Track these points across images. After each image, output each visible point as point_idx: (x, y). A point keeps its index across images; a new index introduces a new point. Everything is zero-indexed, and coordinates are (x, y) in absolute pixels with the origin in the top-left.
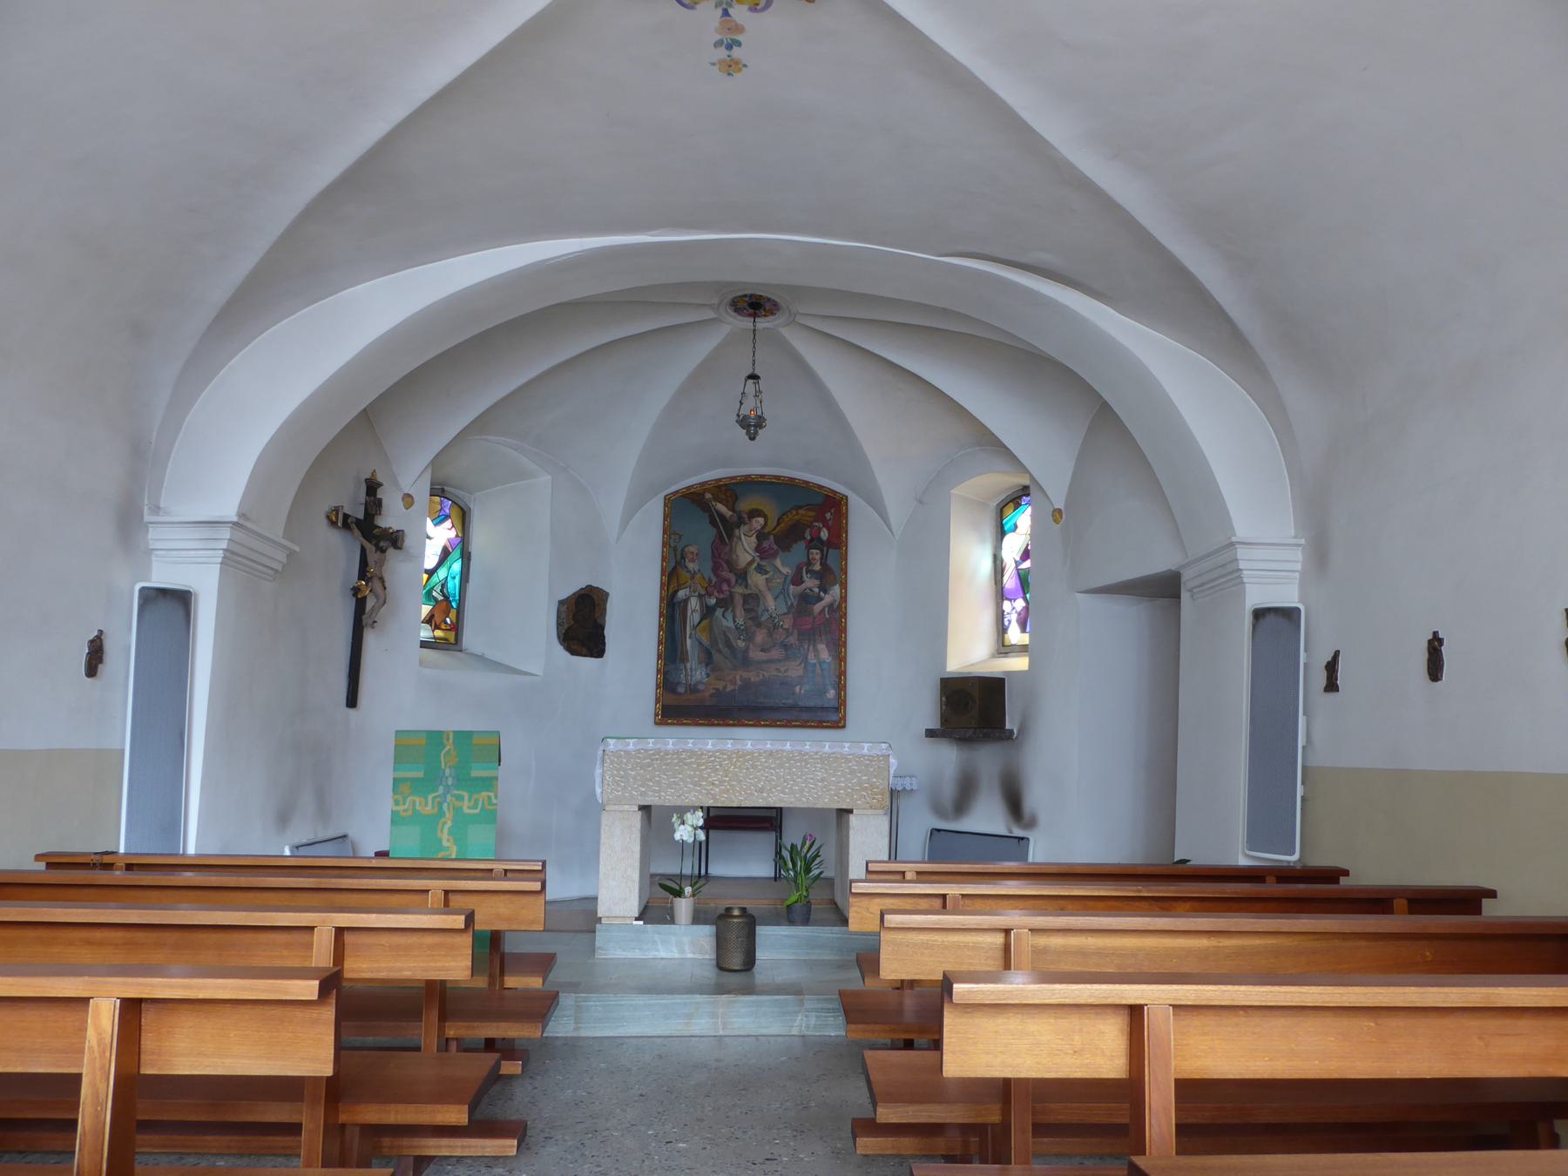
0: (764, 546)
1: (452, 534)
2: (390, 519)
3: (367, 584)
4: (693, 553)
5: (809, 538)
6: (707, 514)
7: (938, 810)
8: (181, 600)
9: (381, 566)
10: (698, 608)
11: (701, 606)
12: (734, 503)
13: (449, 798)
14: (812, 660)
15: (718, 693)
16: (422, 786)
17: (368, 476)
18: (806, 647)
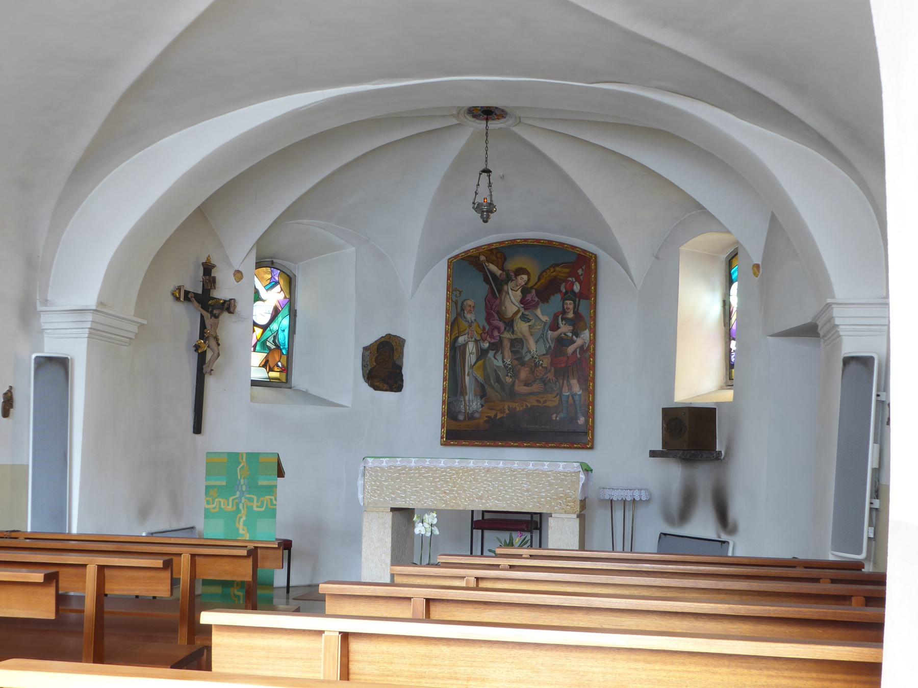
0: (527, 298)
1: (281, 296)
2: (222, 293)
3: (205, 342)
4: (470, 306)
5: (564, 291)
6: (481, 274)
7: (668, 519)
8: (62, 364)
9: (216, 329)
10: (474, 350)
11: (477, 347)
12: (504, 263)
13: (243, 500)
14: (566, 393)
15: (490, 420)
16: (231, 488)
17: (204, 261)
18: (561, 381)
